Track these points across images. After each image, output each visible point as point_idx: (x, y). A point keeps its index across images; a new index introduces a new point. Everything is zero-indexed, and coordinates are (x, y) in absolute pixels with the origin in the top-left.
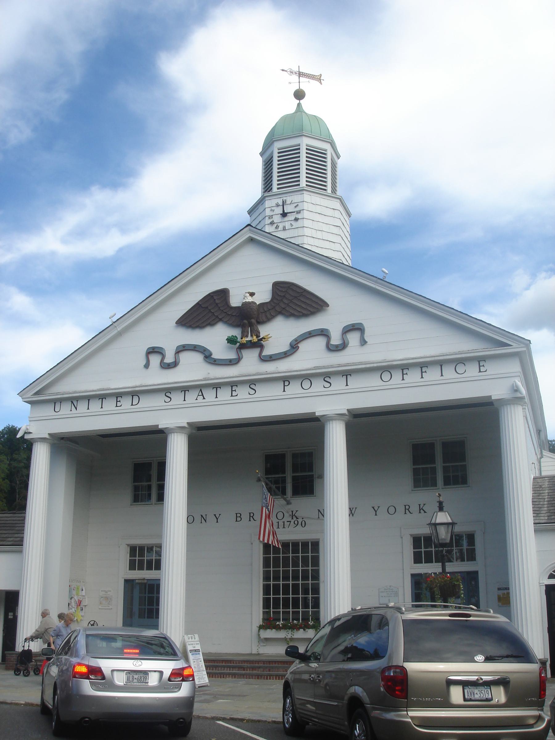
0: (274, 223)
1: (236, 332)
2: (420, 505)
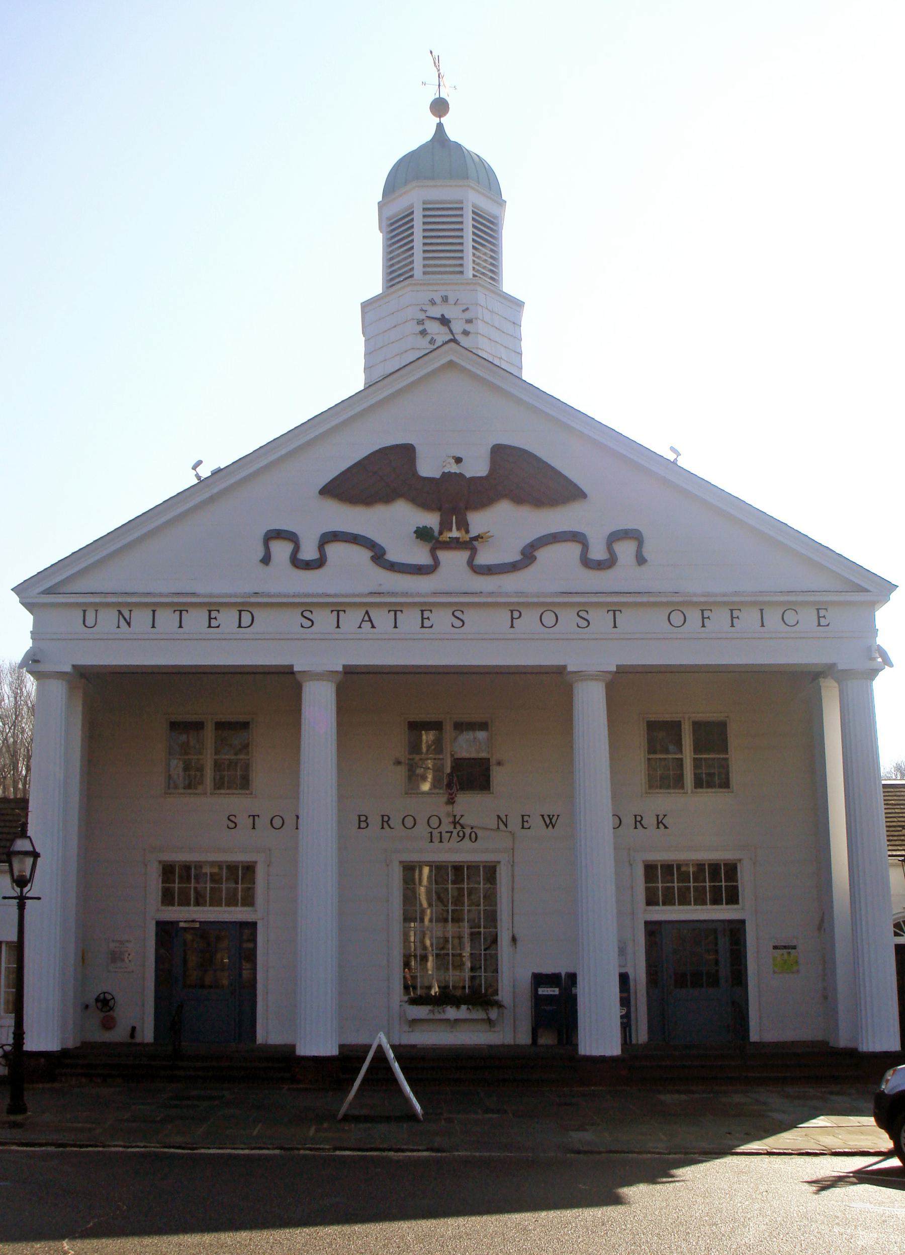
0: (427, 334)
1: (431, 520)
2: (658, 816)
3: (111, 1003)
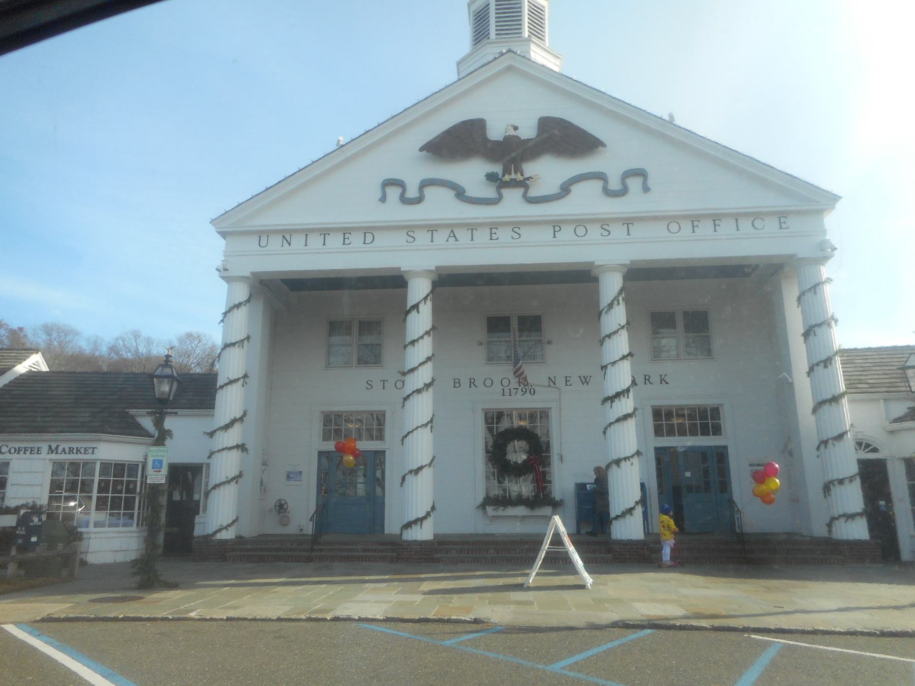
1: (497, 169)
3: (285, 507)
